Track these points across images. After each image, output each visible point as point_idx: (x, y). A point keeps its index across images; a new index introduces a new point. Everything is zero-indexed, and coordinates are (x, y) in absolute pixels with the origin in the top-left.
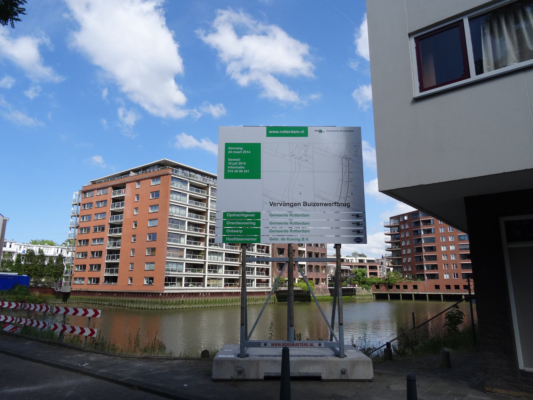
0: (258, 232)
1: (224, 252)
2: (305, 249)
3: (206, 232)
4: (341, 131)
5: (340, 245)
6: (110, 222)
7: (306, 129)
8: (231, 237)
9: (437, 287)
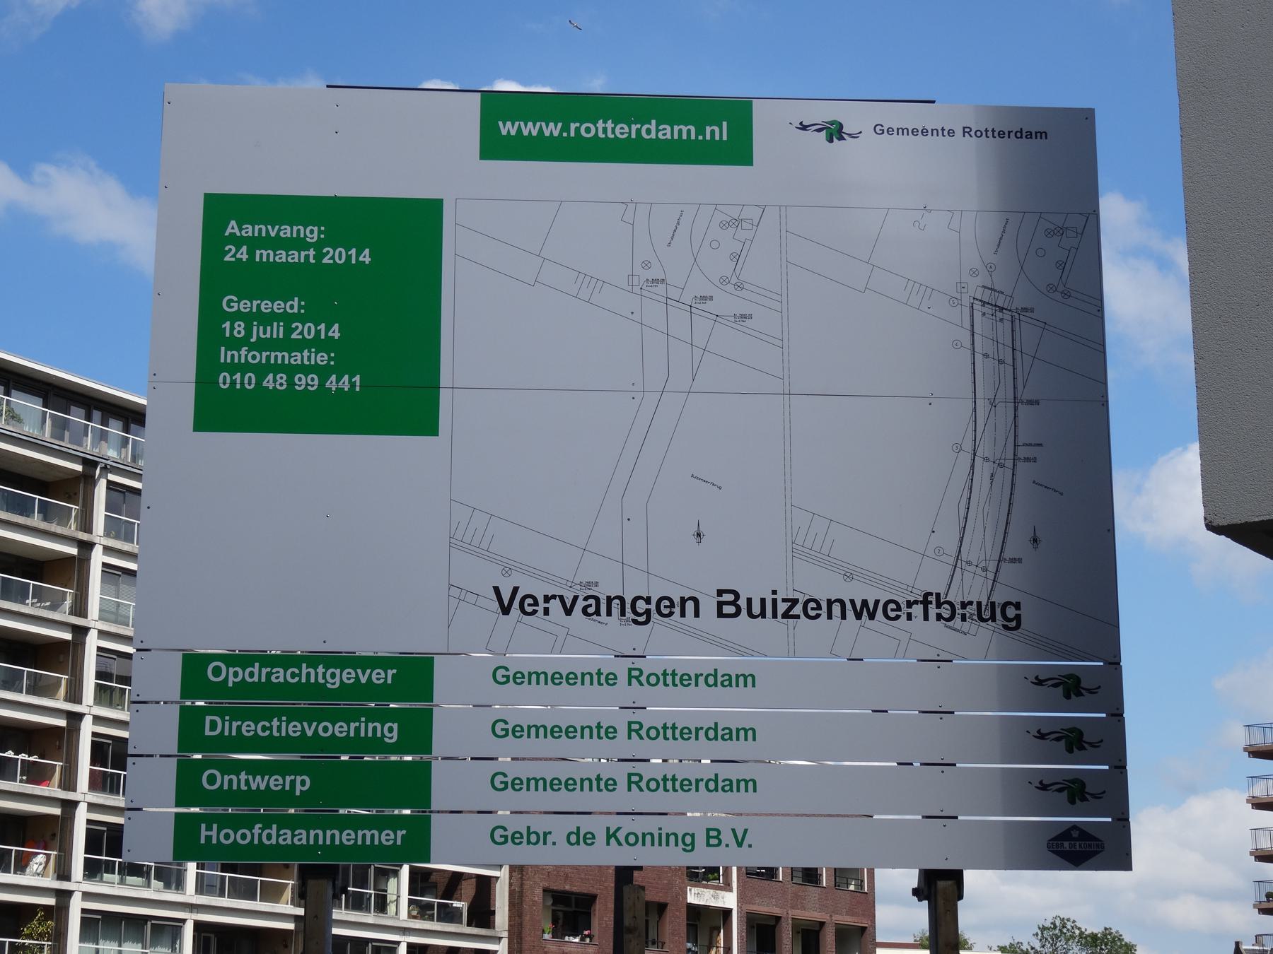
0: (416, 784)
1: (191, 918)
2: (729, 900)
3: (69, 783)
4: (966, 131)
5: (956, 877)
7: (737, 114)
8: (235, 823)
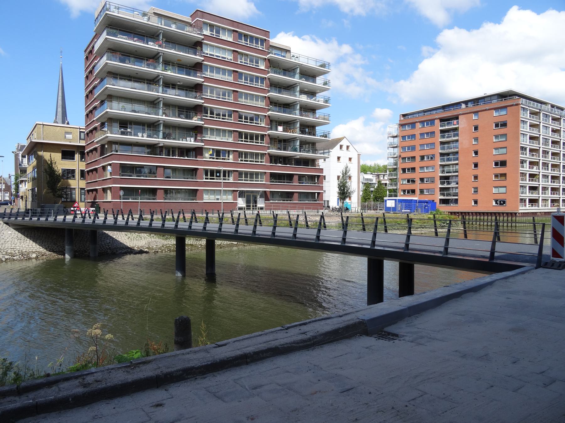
6: (440, 151)
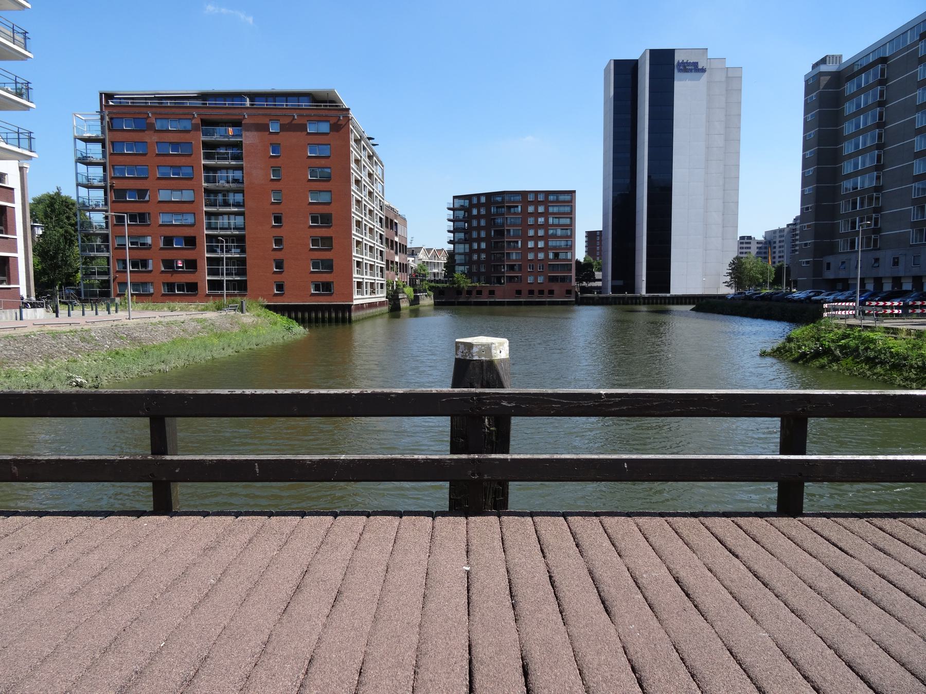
9: (519, 292)
